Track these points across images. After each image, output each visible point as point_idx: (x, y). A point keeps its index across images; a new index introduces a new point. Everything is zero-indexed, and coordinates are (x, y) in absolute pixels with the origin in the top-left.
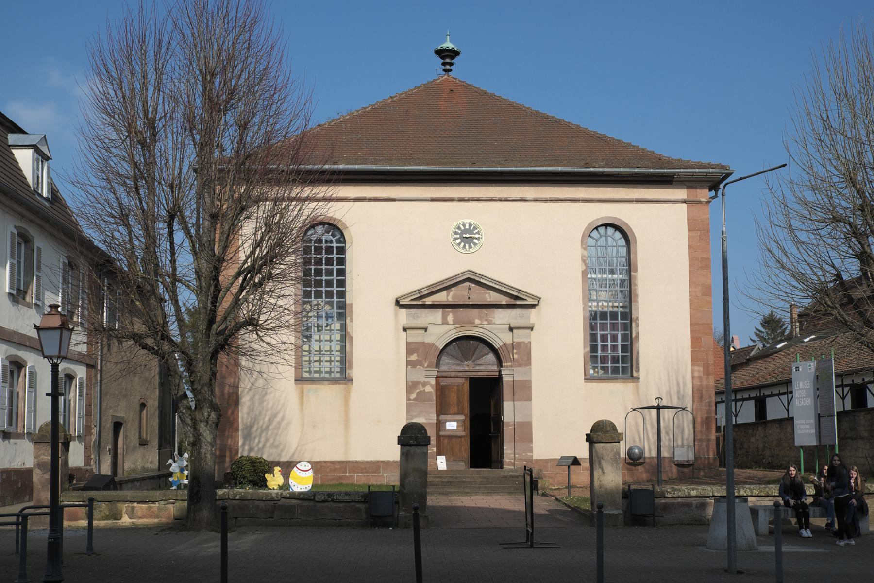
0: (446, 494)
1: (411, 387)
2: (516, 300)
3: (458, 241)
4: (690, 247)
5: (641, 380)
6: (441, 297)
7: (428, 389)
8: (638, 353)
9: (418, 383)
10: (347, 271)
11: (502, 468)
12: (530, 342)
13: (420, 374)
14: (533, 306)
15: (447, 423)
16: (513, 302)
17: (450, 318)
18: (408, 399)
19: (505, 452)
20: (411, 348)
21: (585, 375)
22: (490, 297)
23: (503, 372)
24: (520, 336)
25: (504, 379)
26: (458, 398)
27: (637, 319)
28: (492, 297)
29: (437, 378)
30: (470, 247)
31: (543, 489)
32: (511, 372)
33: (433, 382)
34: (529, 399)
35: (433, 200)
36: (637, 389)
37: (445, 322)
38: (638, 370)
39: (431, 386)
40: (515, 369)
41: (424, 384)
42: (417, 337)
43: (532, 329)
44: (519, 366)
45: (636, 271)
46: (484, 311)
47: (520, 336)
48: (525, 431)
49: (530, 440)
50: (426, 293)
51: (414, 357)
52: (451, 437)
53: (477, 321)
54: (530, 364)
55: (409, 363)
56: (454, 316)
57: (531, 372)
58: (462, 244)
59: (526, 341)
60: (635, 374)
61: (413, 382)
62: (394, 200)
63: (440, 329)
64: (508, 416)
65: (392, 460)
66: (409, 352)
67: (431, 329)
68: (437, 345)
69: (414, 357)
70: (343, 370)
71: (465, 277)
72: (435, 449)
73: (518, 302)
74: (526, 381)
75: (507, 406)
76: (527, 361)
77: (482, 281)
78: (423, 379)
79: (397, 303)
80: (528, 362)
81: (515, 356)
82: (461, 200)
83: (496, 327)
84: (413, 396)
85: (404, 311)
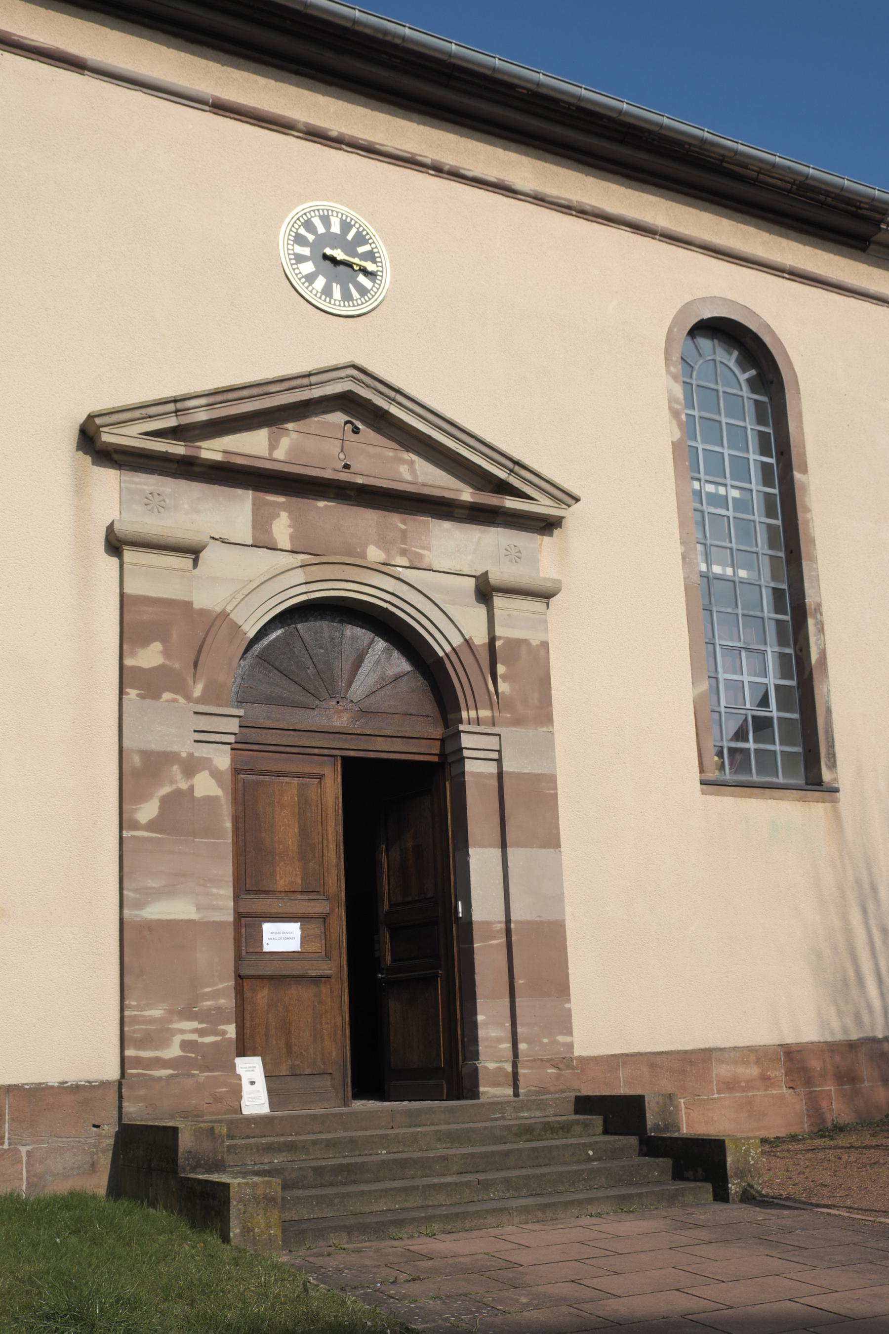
0: (378, 1229)
1: (136, 773)
2: (497, 496)
3: (308, 267)
5: (841, 795)
6: (252, 445)
7: (206, 786)
8: (829, 711)
9: (169, 758)
11: (475, 1095)
12: (545, 645)
13: (170, 726)
14: (547, 525)
15: (267, 927)
16: (493, 500)
17: (282, 529)
19: (481, 1033)
20: (137, 621)
21: (702, 771)
22: (412, 470)
24: (514, 619)
26: (304, 834)
27: (818, 607)
29: (240, 746)
30: (347, 296)
31: (741, 1174)
32: (493, 743)
33: (223, 760)
34: (553, 841)
35: (220, 108)
36: (837, 816)
37: (263, 542)
38: (833, 766)
39: (216, 774)
41: (191, 767)
44: (518, 722)
45: (804, 470)
46: (397, 521)
47: (514, 619)
49: (563, 989)
50: (202, 416)
51: (149, 657)
52: (283, 974)
53: (374, 554)
55: (126, 677)
56: (297, 525)
57: (551, 745)
59: (535, 639)
60: (826, 775)
61: (146, 755)
62: (76, 65)
63: (246, 565)
64: (484, 905)
65: (53, 1079)
66: (130, 635)
68: (238, 617)
69: (149, 657)
72: (231, 1030)
73: (511, 503)
75: (482, 862)
77: (394, 410)
78: (184, 746)
79: (90, 441)
80: (542, 713)
81: (503, 687)
82: (316, 135)
83: (436, 574)
85: (108, 479)
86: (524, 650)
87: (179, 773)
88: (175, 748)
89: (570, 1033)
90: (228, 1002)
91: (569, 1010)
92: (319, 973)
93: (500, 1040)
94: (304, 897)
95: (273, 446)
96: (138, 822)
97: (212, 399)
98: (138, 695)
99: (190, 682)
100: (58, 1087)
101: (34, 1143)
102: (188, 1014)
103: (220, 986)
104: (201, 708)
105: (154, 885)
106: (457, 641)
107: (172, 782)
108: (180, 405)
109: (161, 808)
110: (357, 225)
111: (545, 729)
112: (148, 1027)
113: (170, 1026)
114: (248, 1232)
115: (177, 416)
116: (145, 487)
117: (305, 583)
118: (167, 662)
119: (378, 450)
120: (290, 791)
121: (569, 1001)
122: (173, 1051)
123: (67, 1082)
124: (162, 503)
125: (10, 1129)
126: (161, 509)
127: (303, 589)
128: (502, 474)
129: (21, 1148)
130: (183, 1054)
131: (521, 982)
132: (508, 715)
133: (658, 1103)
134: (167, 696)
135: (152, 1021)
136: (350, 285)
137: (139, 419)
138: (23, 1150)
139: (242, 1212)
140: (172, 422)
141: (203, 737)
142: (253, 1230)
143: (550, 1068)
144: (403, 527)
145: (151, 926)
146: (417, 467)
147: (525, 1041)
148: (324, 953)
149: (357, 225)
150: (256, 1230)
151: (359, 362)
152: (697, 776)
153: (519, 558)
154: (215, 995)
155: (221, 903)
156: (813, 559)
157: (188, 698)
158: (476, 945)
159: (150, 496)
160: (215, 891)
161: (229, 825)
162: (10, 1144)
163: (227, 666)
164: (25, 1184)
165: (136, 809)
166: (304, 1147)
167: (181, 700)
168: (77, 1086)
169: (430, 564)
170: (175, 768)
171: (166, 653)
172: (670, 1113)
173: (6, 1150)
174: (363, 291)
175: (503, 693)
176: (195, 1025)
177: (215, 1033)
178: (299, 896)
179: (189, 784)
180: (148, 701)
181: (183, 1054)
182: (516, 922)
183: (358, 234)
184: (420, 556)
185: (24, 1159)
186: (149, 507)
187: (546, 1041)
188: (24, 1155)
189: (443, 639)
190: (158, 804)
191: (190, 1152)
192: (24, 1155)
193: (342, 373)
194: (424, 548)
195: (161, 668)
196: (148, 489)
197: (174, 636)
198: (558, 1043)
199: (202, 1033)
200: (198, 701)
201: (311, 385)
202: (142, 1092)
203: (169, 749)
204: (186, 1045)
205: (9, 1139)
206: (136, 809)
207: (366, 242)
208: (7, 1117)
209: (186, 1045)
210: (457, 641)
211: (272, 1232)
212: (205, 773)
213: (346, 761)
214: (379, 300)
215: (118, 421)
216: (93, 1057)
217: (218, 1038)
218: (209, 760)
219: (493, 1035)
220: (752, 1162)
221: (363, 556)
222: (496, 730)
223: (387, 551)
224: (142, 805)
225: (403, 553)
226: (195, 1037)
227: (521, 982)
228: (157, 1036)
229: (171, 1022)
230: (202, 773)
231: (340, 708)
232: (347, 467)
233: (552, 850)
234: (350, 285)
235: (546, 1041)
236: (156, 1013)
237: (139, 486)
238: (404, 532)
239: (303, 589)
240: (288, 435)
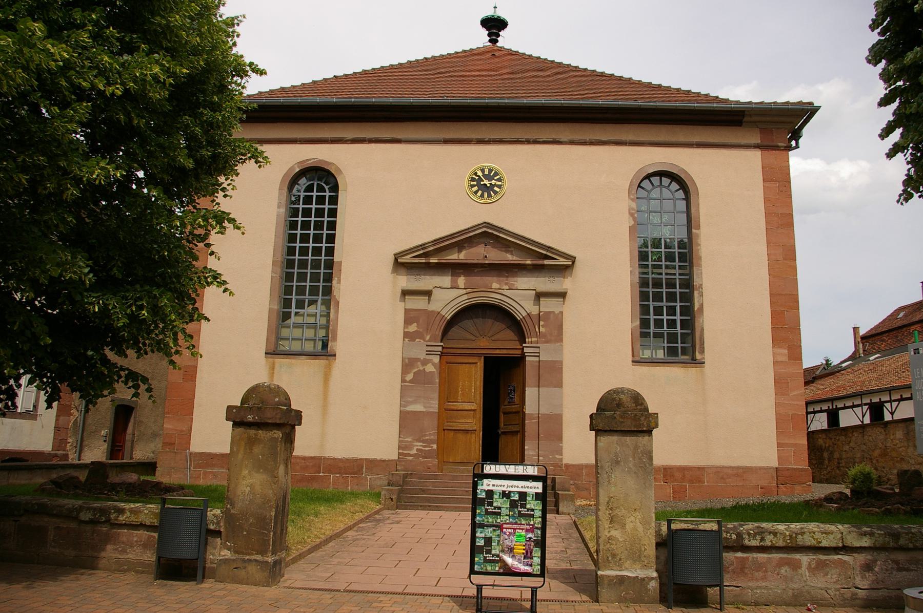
1: (408, 364)
2: (545, 262)
4: (766, 200)
7: (430, 368)
8: (702, 329)
9: (417, 360)
12: (562, 313)
18: (403, 381)
20: (410, 317)
21: (633, 356)
23: (525, 350)
33: (436, 359)
34: (559, 384)
37: (455, 287)
39: (434, 364)
41: (425, 362)
44: (547, 342)
45: (698, 228)
49: (560, 439)
51: (413, 328)
55: (406, 335)
60: (698, 356)
61: (409, 359)
63: (447, 295)
64: (530, 408)
66: (408, 321)
69: (413, 328)
71: (480, 231)
73: (547, 262)
78: (422, 356)
82: (480, 142)
83: (519, 294)
84: (409, 377)
93: (534, 455)
104: (429, 343)
106: (524, 314)
122: (414, 452)
123: (27, 461)
135: (407, 442)
140: (422, 252)
141: (429, 353)
145: (408, 412)
152: (630, 359)
154: (430, 435)
156: (700, 265)
157: (424, 340)
161: (437, 380)
171: (418, 327)
174: (496, 193)
189: (520, 314)
200: (429, 341)
210: (524, 314)
213: (485, 358)
216: (775, 464)
225: (506, 284)
236: (409, 439)
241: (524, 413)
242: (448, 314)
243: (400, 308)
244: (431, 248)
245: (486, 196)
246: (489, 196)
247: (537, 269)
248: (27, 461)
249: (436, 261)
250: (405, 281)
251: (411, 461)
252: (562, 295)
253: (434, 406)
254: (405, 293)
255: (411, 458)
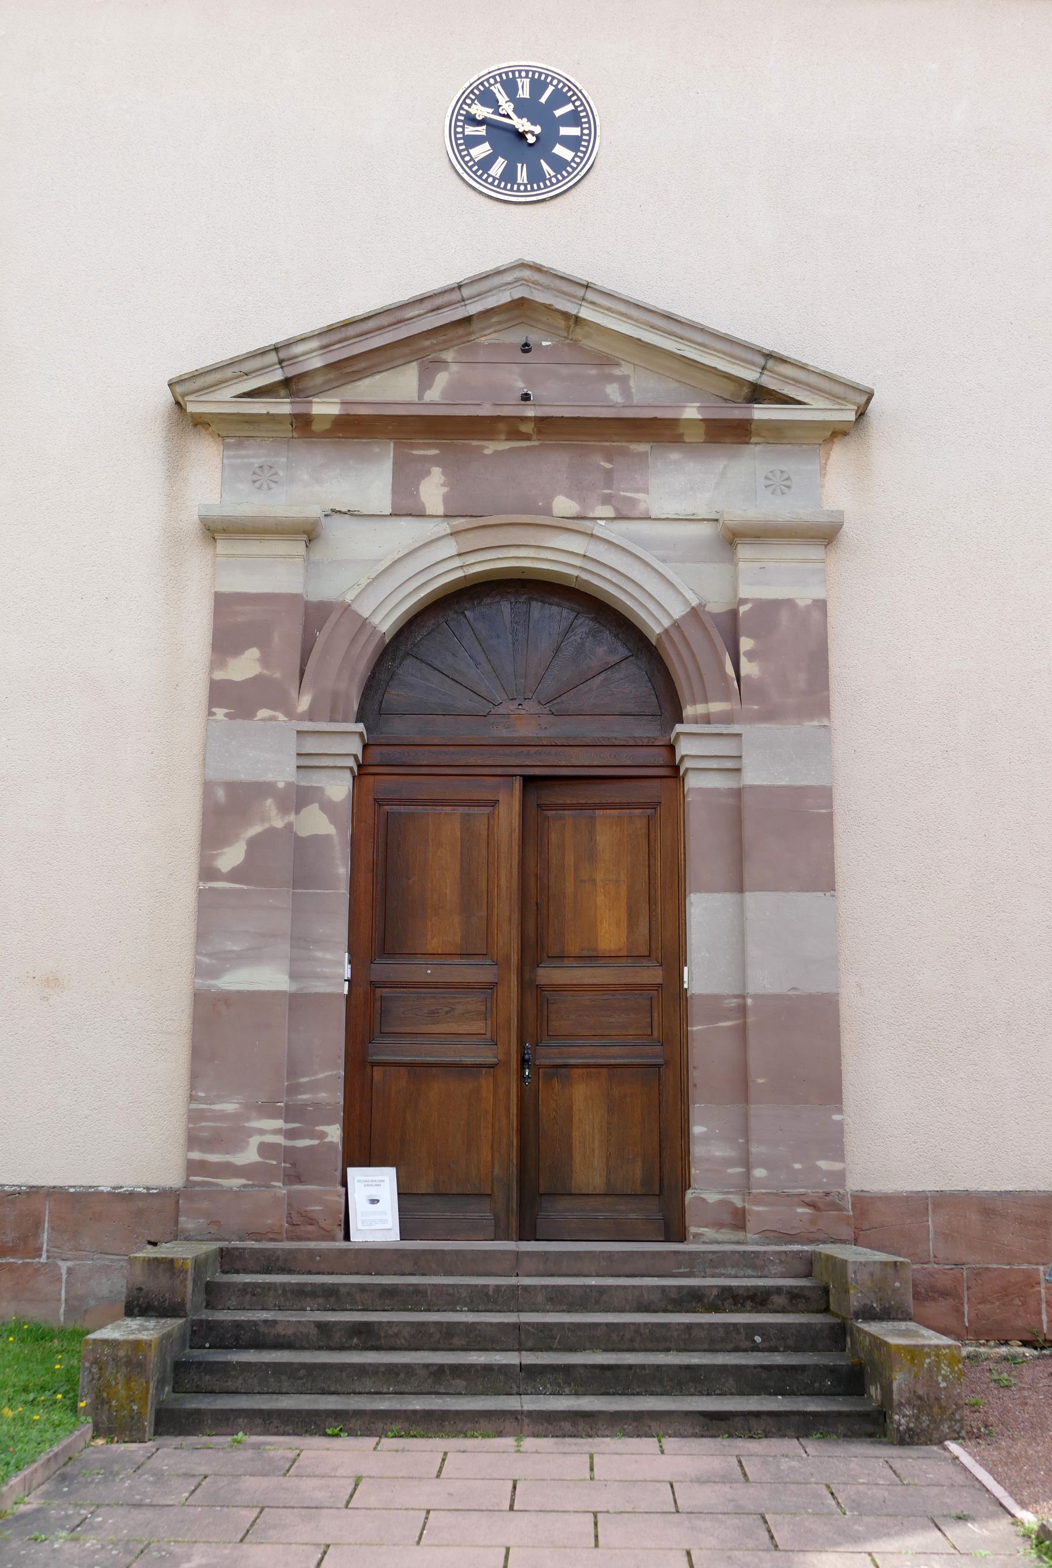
1: (226, 808)
2: (750, 407)
6: (398, 388)
7: (316, 823)
9: (262, 789)
10: (181, 1138)
12: (821, 605)
13: (268, 753)
14: (837, 433)
17: (433, 491)
18: (207, 872)
19: (697, 1151)
20: (234, 623)
22: (626, 391)
23: (684, 748)
24: (766, 578)
25: (693, 782)
28: (639, 392)
33: (339, 788)
34: (822, 879)
37: (406, 509)
39: (328, 807)
40: (752, 732)
42: (272, 573)
43: (298, 767)
44: (770, 715)
48: (803, 1049)
49: (831, 1093)
51: (245, 667)
53: (563, 505)
54: (823, 708)
55: (220, 694)
56: (453, 482)
58: (498, 167)
59: (803, 595)
61: (233, 788)
63: (385, 545)
65: (105, 1185)
66: (226, 641)
67: (338, 531)
68: (364, 610)
69: (245, 667)
70: (945, 1294)
71: (504, 298)
72: (334, 1133)
73: (761, 412)
74: (799, 793)
76: (807, 688)
78: (281, 771)
81: (747, 668)
83: (653, 539)
84: (231, 857)
86: (784, 616)
87: (273, 807)
88: (269, 777)
89: (839, 1154)
90: (334, 1096)
91: (840, 1125)
92: (479, 1060)
93: (729, 1162)
94: (463, 961)
95: (425, 384)
96: (218, 870)
97: (326, 340)
98: (226, 715)
99: (294, 693)
100: (108, 1193)
101: (76, 1259)
102: (267, 1110)
103: (321, 1076)
105: (234, 948)
107: (263, 820)
108: (283, 354)
109: (248, 853)
110: (555, 82)
111: (815, 723)
112: (219, 1124)
113: (246, 1124)
114: (102, 1405)
115: (282, 367)
116: (254, 460)
117: (459, 555)
118: (265, 672)
119: (574, 370)
120: (448, 826)
121: (840, 1111)
122: (249, 1156)
123: (121, 1187)
124: (274, 478)
125: (49, 1240)
126: (273, 485)
127: (457, 562)
128: (750, 375)
129: (61, 1263)
130: (260, 1160)
131: (760, 1081)
132: (756, 707)
133: (872, 1274)
134: (263, 713)
135: (223, 1116)
136: (542, 161)
137: (232, 379)
138: (64, 1266)
139: (96, 1377)
142: (109, 1402)
143: (800, 1206)
144: (608, 466)
145: (227, 999)
146: (632, 383)
147: (762, 1164)
148: (489, 1035)
149: (555, 82)
150: (114, 1403)
151: (528, 258)
153: (254, 482)
155: (326, 970)
157: (290, 714)
158: (695, 1028)
159: (258, 471)
160: (319, 954)
162: (48, 1258)
163: (344, 671)
164: (63, 1306)
165: (217, 854)
166: (349, 1294)
167: (281, 717)
168: (131, 1194)
169: (647, 510)
170: (269, 802)
171: (264, 661)
172: (895, 1290)
173: (43, 1264)
175: (748, 676)
176: (279, 1124)
177: (312, 1135)
178: (457, 961)
179: (286, 821)
180: (239, 721)
181: (260, 1160)
182: (755, 997)
183: (557, 92)
184: (633, 502)
185: (64, 1277)
186: (257, 484)
187: (797, 1166)
188: (64, 1271)
189: (659, 608)
190: (245, 847)
191: (140, 1289)
192: (64, 1271)
193: (509, 278)
194: (638, 490)
195: (257, 679)
196: (256, 462)
197: (276, 638)
198: (818, 1169)
199: (290, 1134)
200: (301, 718)
201: (463, 300)
202: (205, 1205)
203: (262, 779)
204: (264, 1149)
205: (47, 1251)
206: (217, 854)
207: (568, 100)
208: (46, 1225)
209: (264, 1149)
211: (135, 1407)
212: (316, 806)
214: (582, 173)
215: (206, 385)
217: (315, 1142)
218: (320, 790)
219: (718, 1154)
220: (943, 1385)
221: (547, 511)
222: (735, 729)
223: (582, 501)
224: (225, 850)
225: (607, 500)
226: (279, 1139)
227: (760, 1081)
228: (228, 1136)
229: (248, 1119)
230: (310, 807)
231: (523, 712)
232: (526, 397)
233: (821, 894)
234: (542, 161)
235: (797, 1166)
236: (230, 1107)
237: (246, 460)
238: (609, 473)
239: (457, 562)
240: (446, 369)
241: (680, 996)
242: (385, 616)
243: (202, 577)
244: (317, 363)
245: (522, 175)
246: (536, 177)
247: (729, 433)
248: (121, 1187)
249: (335, 410)
250: (210, 481)
251: (237, 1194)
252: (826, 535)
253: (335, 971)
254: (215, 531)
255: (236, 1183)
